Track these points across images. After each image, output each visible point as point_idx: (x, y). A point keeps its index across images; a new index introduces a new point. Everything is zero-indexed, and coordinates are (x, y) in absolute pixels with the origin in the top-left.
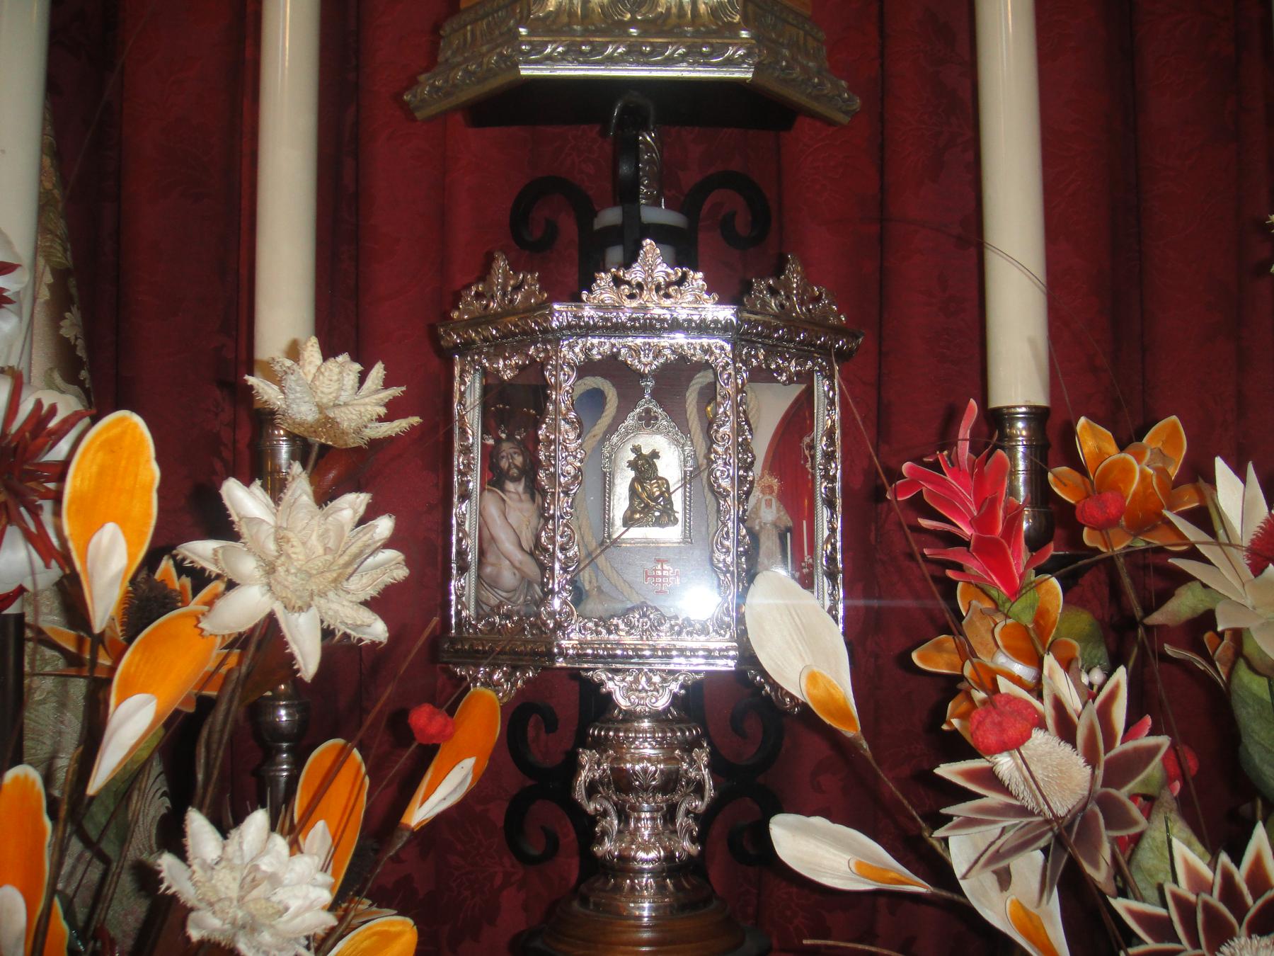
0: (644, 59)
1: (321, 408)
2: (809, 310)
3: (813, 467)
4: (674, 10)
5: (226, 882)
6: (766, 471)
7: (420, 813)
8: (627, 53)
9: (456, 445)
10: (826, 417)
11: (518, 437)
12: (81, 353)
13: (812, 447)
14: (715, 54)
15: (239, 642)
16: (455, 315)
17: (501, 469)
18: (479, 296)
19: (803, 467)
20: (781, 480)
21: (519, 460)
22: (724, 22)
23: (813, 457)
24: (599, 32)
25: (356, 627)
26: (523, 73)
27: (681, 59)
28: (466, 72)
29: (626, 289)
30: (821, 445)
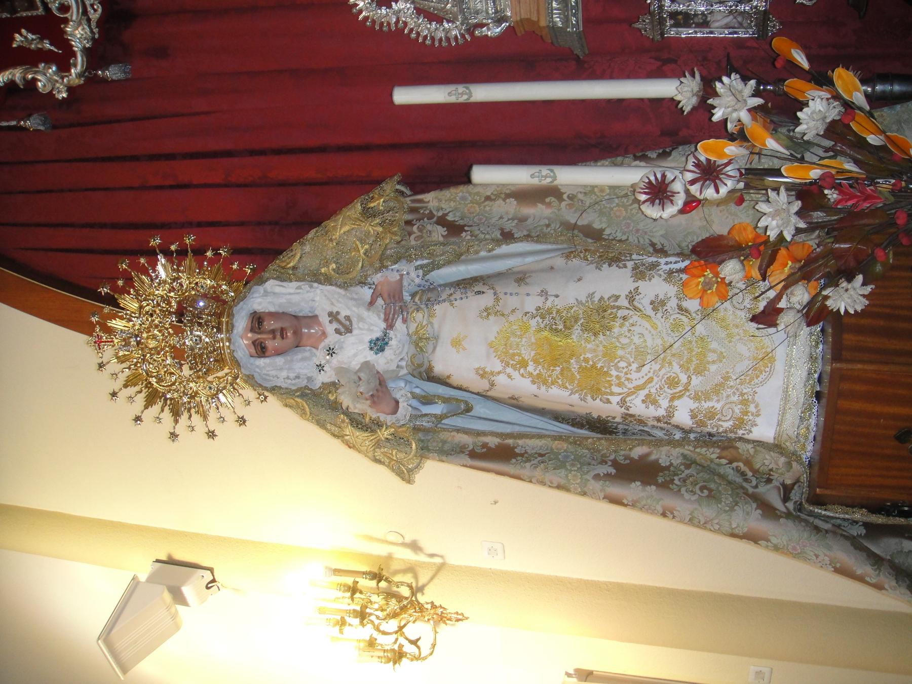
1: (693, 95)
5: (812, 124)
7: (805, 65)
12: (661, 151)
15: (754, 119)
16: (651, 37)
18: (646, 31)
24: (567, 6)
25: (752, 88)
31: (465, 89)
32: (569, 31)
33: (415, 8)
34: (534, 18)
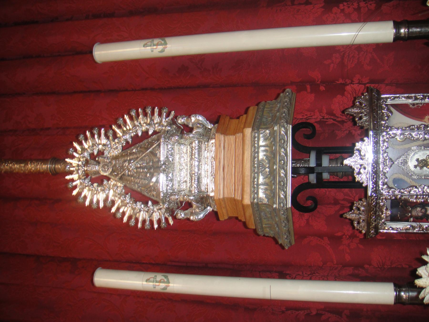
0: (286, 163)
2: (365, 106)
3: (421, 104)
4: (265, 153)
6: (423, 120)
8: (284, 169)
9: (411, 231)
10: (402, 100)
11: (410, 209)
13: (414, 105)
14: (284, 138)
17: (422, 215)
18: (359, 223)
19: (421, 107)
20: (426, 115)
21: (419, 209)
22: (269, 136)
23: (417, 104)
26: (290, 206)
27: (286, 150)
28: (285, 227)
29: (362, 171)
30: (410, 101)
31: (163, 278)
32: (276, 208)
33: (125, 187)
34: (239, 198)
